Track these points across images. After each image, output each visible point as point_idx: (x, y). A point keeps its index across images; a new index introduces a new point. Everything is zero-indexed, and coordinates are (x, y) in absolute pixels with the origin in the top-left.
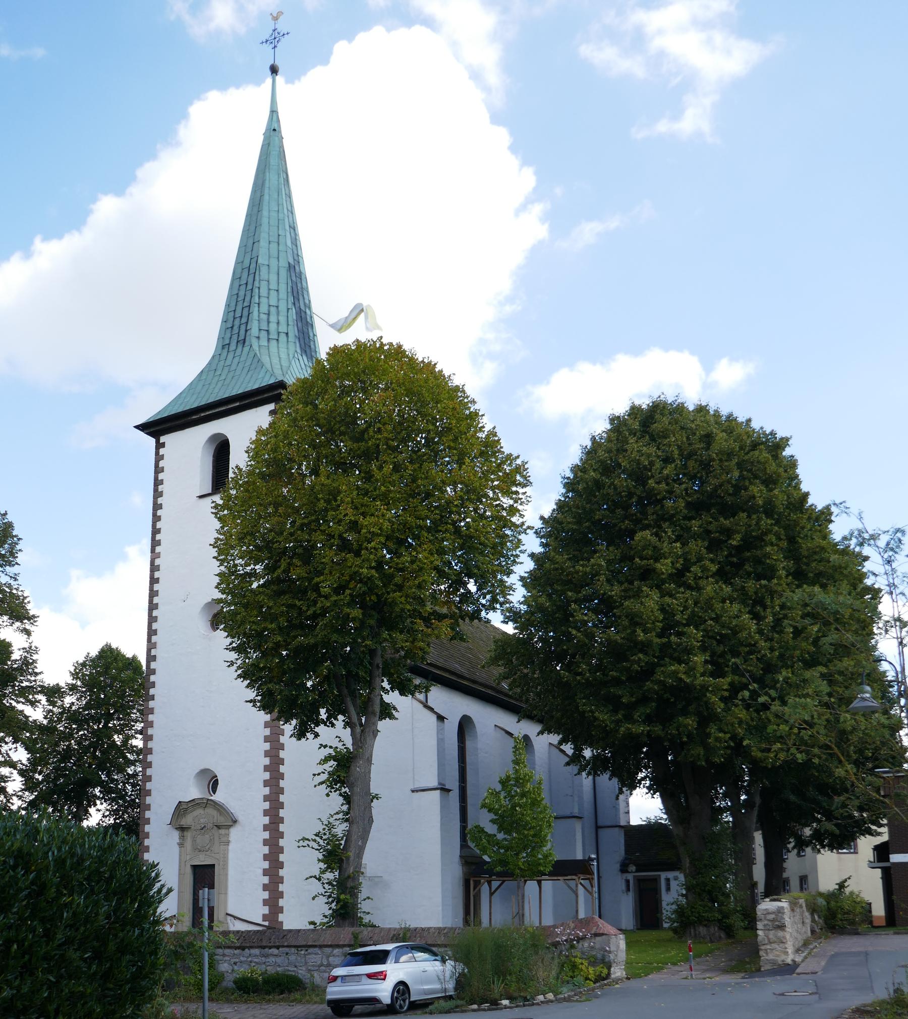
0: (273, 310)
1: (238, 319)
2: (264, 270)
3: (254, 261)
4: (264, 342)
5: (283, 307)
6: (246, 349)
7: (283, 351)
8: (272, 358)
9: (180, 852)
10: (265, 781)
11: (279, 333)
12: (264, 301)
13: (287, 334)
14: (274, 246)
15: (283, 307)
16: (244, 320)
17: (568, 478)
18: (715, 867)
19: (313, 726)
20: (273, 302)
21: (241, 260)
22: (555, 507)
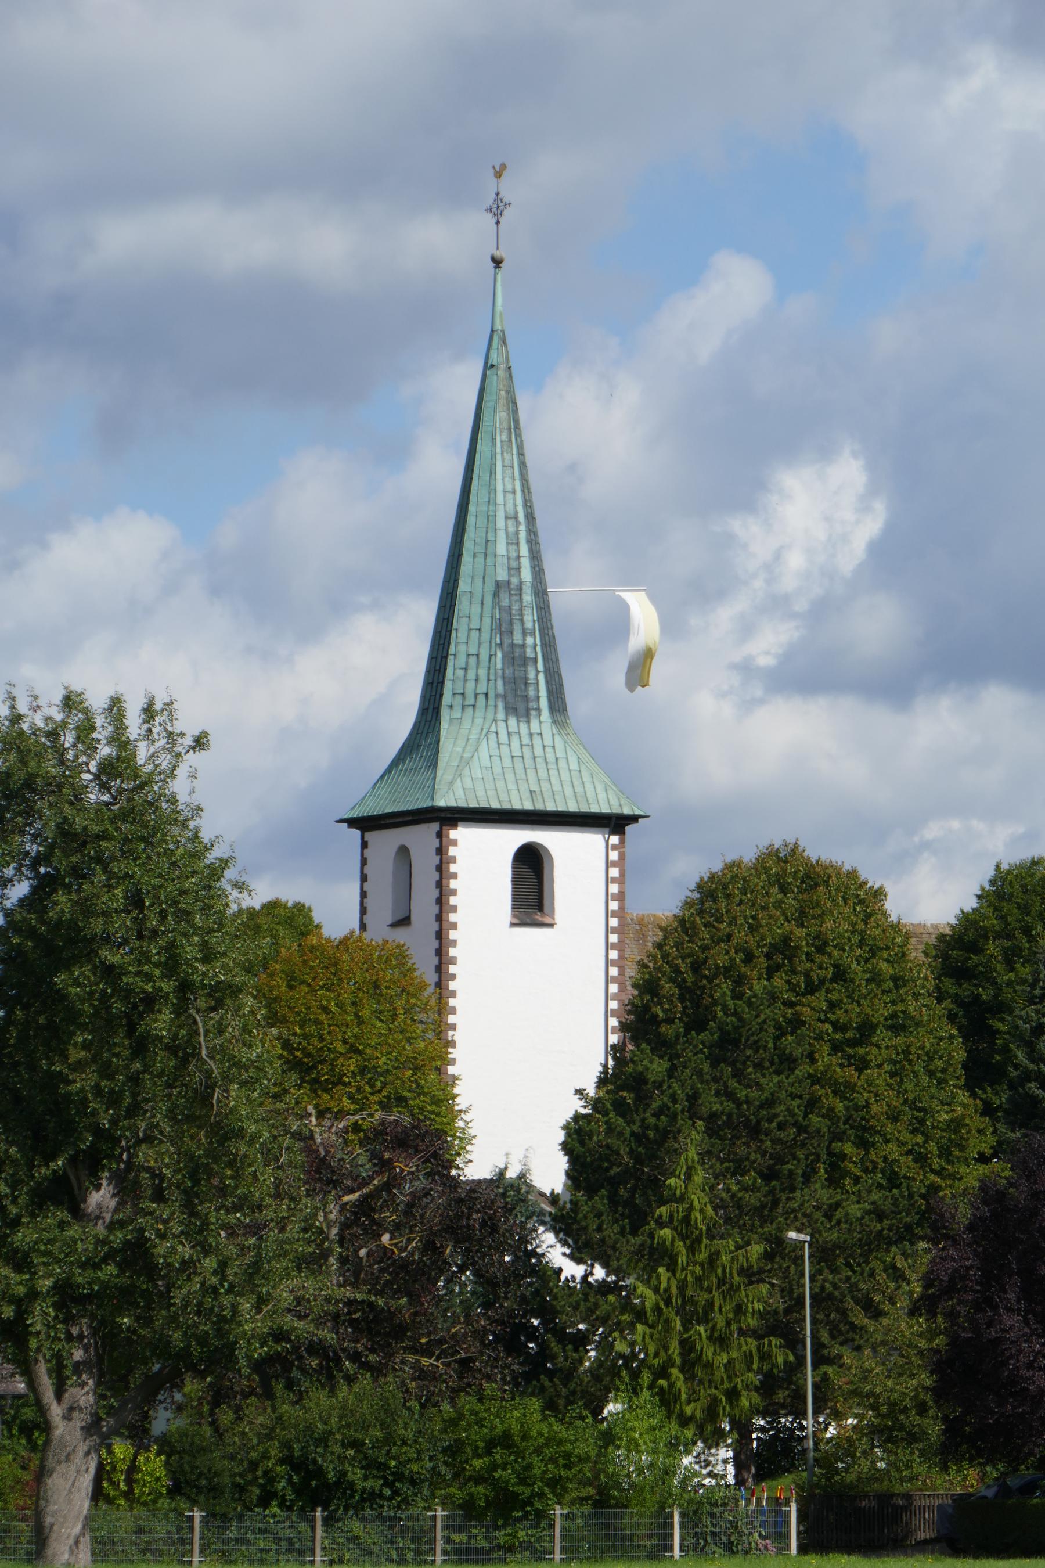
0: (472, 661)
10: (455, 862)
13: (486, 694)
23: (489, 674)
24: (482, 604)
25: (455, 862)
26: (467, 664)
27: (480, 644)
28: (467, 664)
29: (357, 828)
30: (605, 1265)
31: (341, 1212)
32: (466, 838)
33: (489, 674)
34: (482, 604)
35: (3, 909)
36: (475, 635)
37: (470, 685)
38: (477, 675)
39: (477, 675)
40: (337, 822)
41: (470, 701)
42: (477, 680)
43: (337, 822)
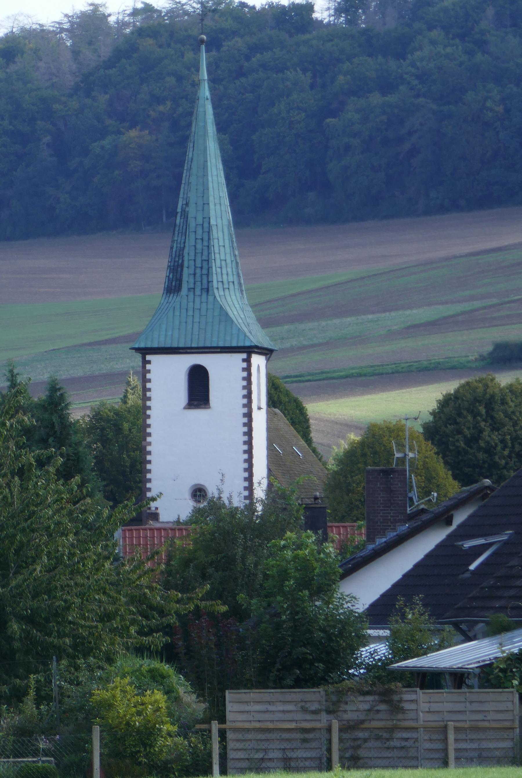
0: (223, 263)
1: (199, 255)
2: (214, 229)
3: (206, 220)
4: (222, 293)
5: (229, 261)
6: (211, 298)
7: (233, 297)
8: (232, 296)
9: (170, 522)
10: (150, 473)
11: (229, 282)
12: (217, 256)
13: (233, 282)
14: (218, 207)
15: (229, 261)
16: (205, 272)
17: (154, 499)
18: (28, 431)
19: (81, 421)
20: (223, 258)
21: (206, 206)
22: (452, 392)
23: (233, 271)
24: (223, 232)
25: (150, 473)
26: (221, 264)
27: (225, 254)
28: (221, 264)
29: (140, 353)
30: (319, 530)
31: (180, 736)
32: (158, 363)
33: (233, 271)
34: (223, 232)
35: (2, 395)
36: (222, 249)
37: (225, 277)
38: (227, 272)
39: (227, 272)
40: (258, 365)
41: (226, 286)
42: (227, 274)
43: (258, 365)
